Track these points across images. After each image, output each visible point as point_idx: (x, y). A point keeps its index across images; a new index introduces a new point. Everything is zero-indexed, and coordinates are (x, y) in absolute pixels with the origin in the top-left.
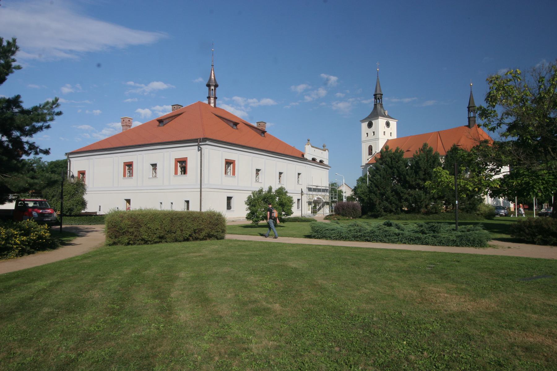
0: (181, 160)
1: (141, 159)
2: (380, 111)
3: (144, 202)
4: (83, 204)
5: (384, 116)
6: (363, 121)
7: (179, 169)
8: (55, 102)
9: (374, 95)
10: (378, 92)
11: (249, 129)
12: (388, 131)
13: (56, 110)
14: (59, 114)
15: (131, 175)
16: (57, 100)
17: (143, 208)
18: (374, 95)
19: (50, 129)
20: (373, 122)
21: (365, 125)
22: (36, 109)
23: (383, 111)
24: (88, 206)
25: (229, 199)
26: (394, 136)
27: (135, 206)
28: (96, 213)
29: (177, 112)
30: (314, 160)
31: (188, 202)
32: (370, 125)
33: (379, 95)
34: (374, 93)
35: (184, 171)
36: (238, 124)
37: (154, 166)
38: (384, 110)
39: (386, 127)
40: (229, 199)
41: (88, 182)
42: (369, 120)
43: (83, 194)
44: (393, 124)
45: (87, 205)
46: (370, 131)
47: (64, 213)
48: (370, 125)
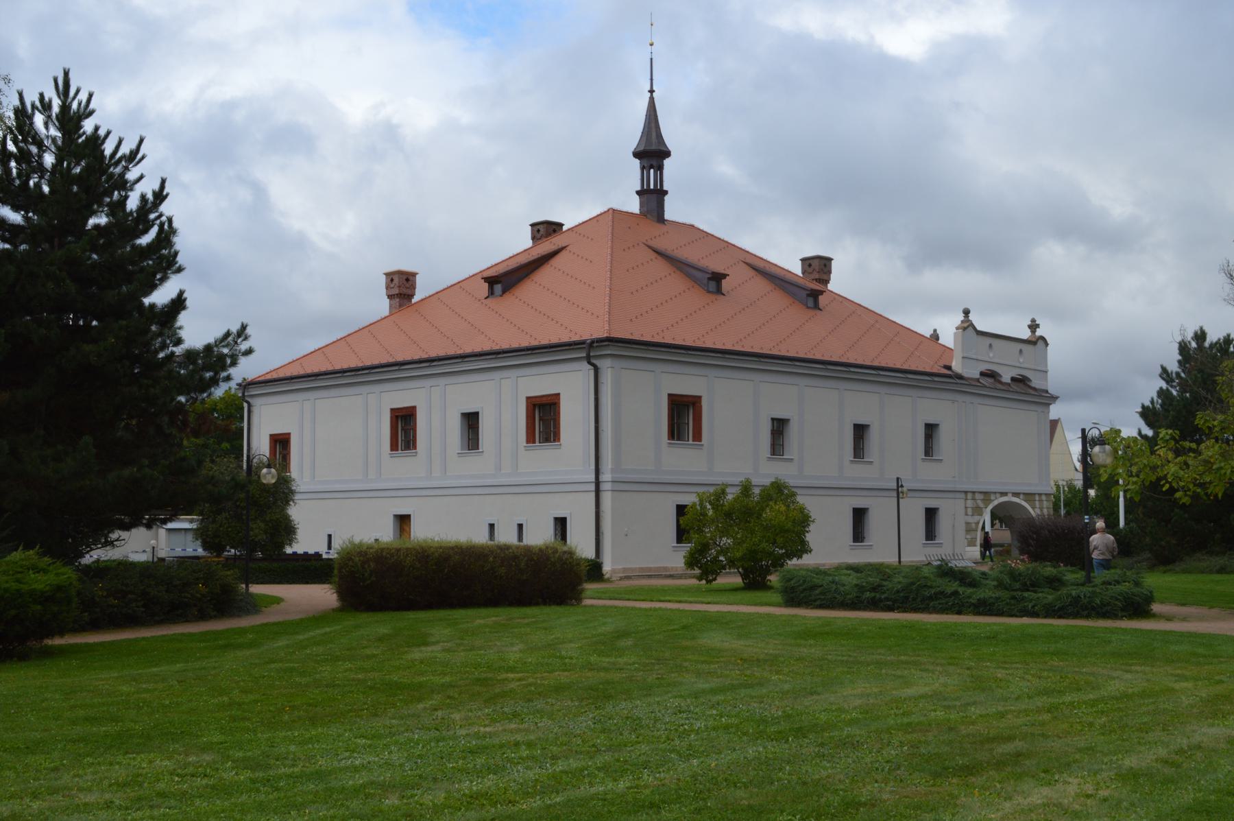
0: (544, 401)
1: (439, 404)
3: (446, 524)
4: (287, 530)
8: (242, 332)
11: (761, 285)
13: (244, 346)
14: (249, 352)
16: (244, 327)
17: (357, 540)
19: (183, 274)
22: (208, 348)
24: (301, 534)
27: (421, 532)
28: (318, 555)
29: (546, 247)
30: (991, 375)
31: (492, 526)
36: (724, 276)
41: (299, 471)
43: (287, 503)
45: (298, 531)
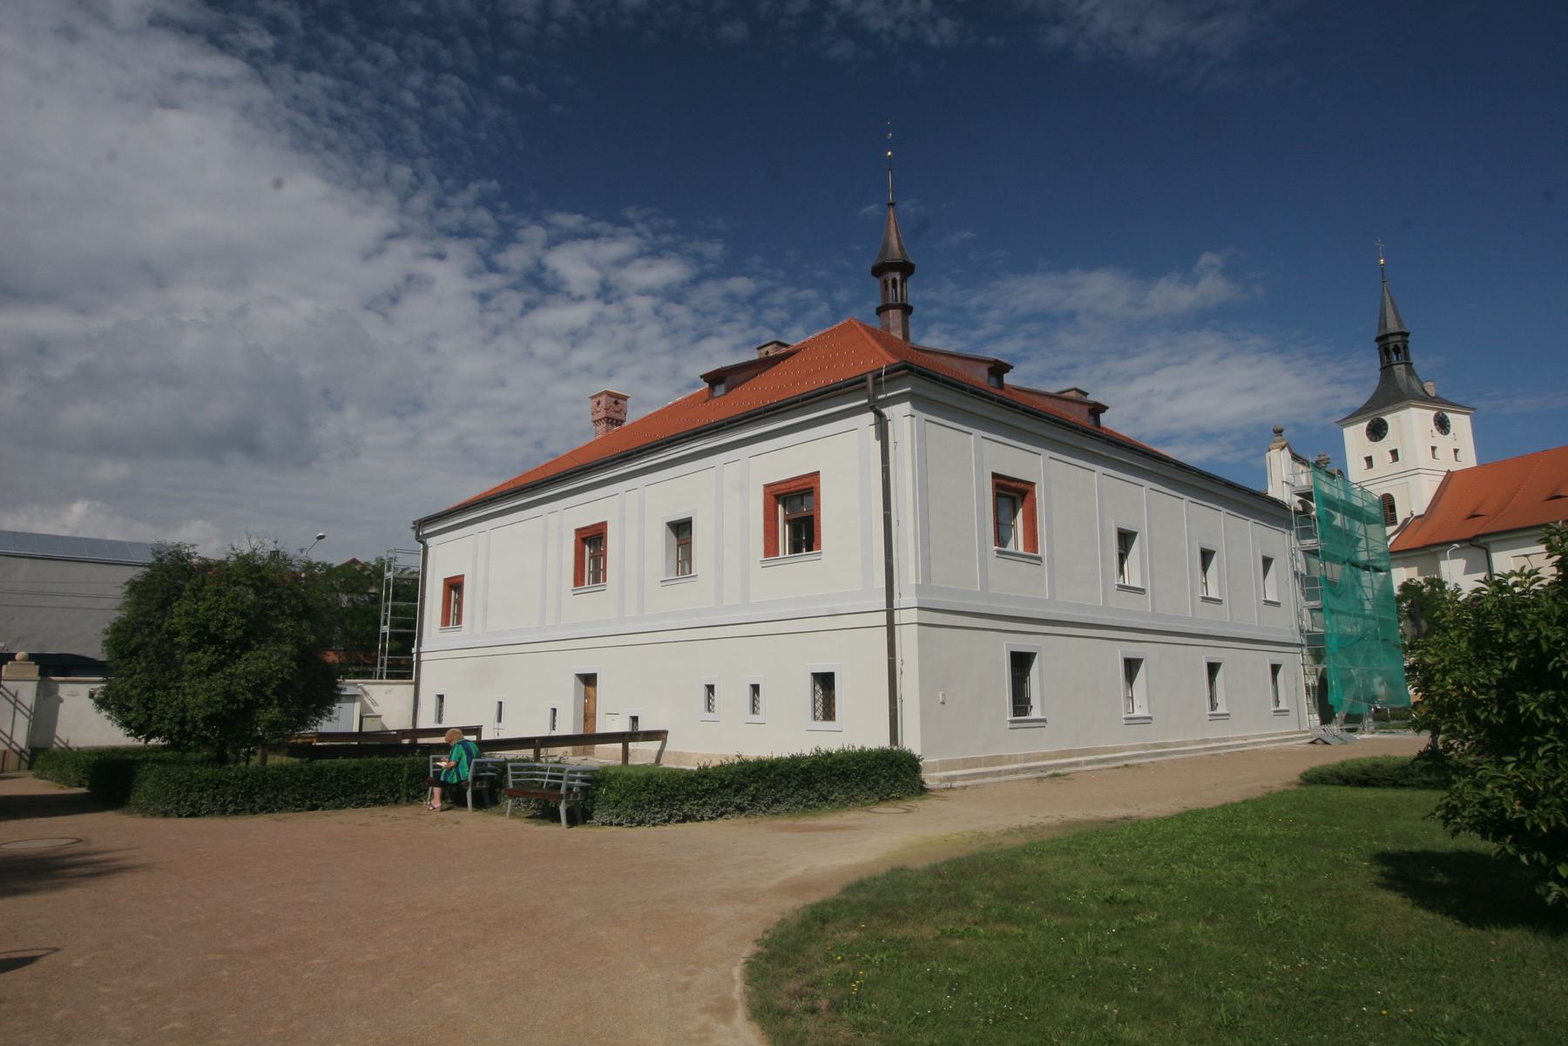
1: (634, 507)
2: (1409, 386)
5: (1424, 399)
6: (1354, 417)
7: (784, 532)
9: (1378, 340)
10: (1392, 326)
12: (1444, 443)
15: (599, 575)
18: (1378, 340)
20: (1388, 418)
21: (1355, 435)
23: (1416, 385)
25: (1021, 663)
26: (1469, 460)
32: (1377, 431)
33: (1398, 338)
34: (1376, 334)
35: (805, 535)
37: (681, 529)
38: (1421, 384)
39: (1437, 433)
40: (1021, 663)
42: (1373, 415)
44: (1460, 423)
46: (1380, 450)
47: (214, 755)
48: (1377, 431)
